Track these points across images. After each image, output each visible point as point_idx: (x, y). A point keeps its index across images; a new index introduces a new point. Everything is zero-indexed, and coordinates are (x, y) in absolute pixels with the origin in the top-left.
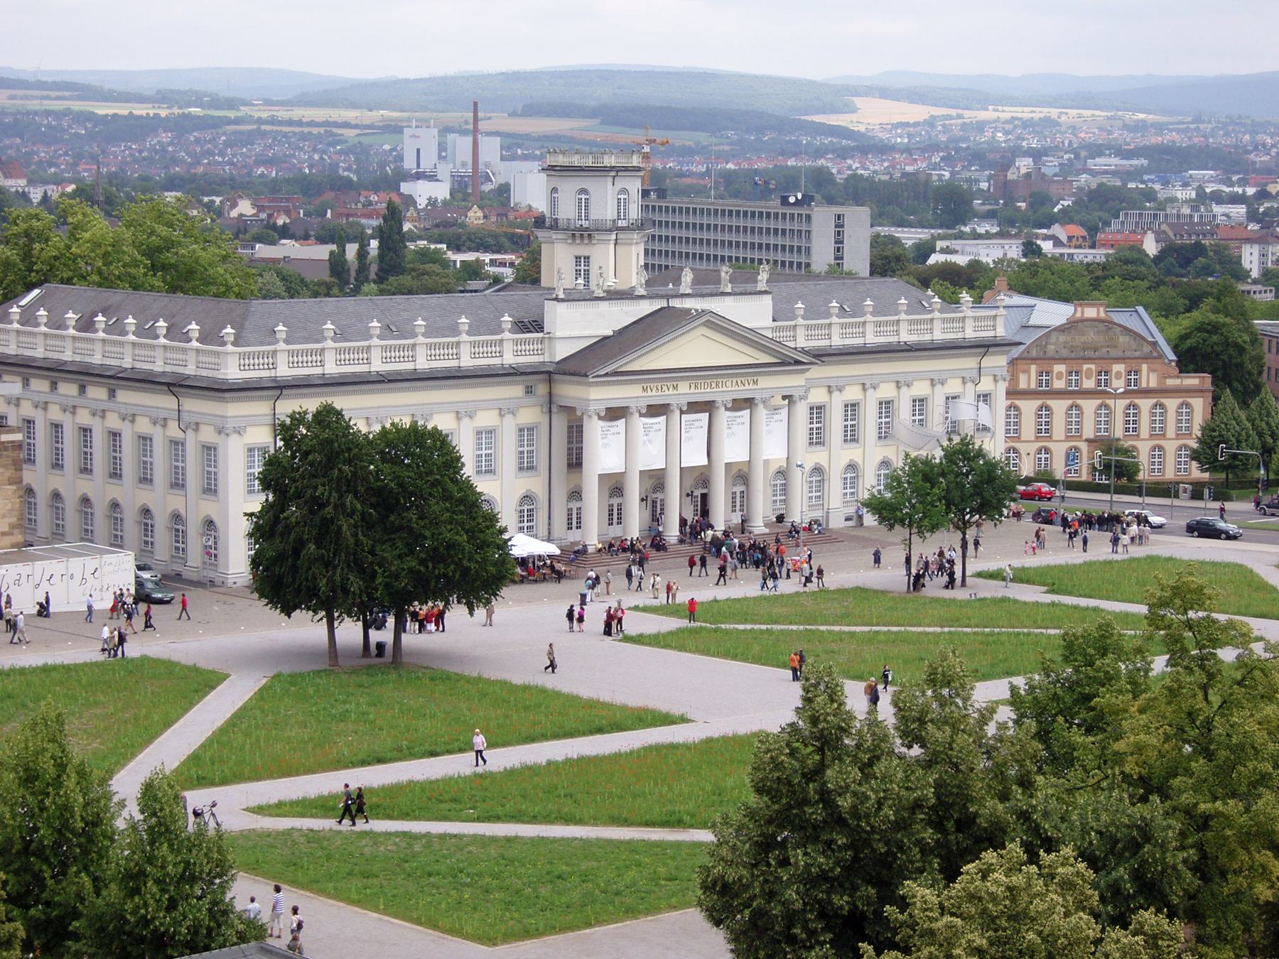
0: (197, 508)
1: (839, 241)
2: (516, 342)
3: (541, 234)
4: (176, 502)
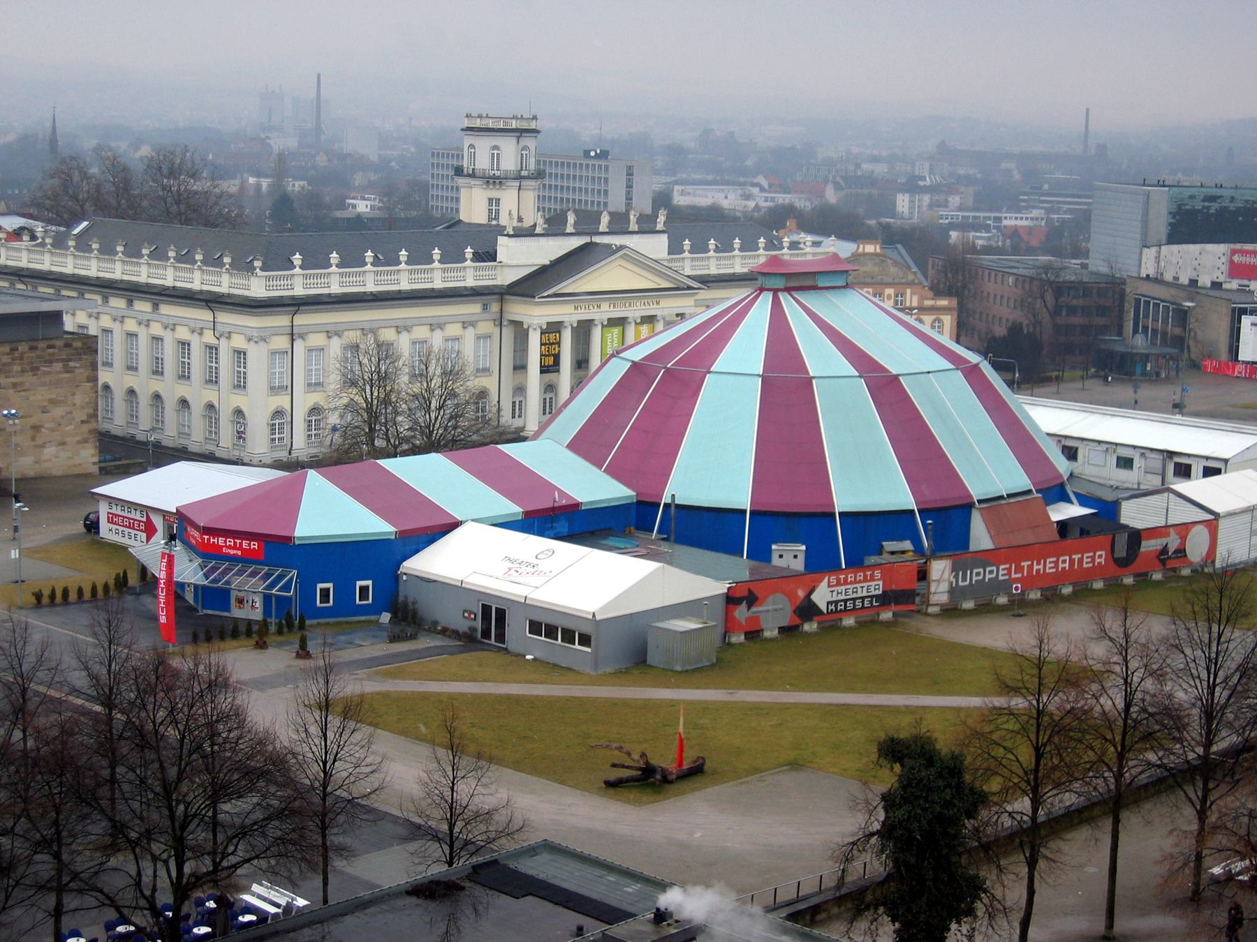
0: (228, 400)
1: (629, 186)
2: (476, 269)
3: (461, 181)
4: (210, 395)
